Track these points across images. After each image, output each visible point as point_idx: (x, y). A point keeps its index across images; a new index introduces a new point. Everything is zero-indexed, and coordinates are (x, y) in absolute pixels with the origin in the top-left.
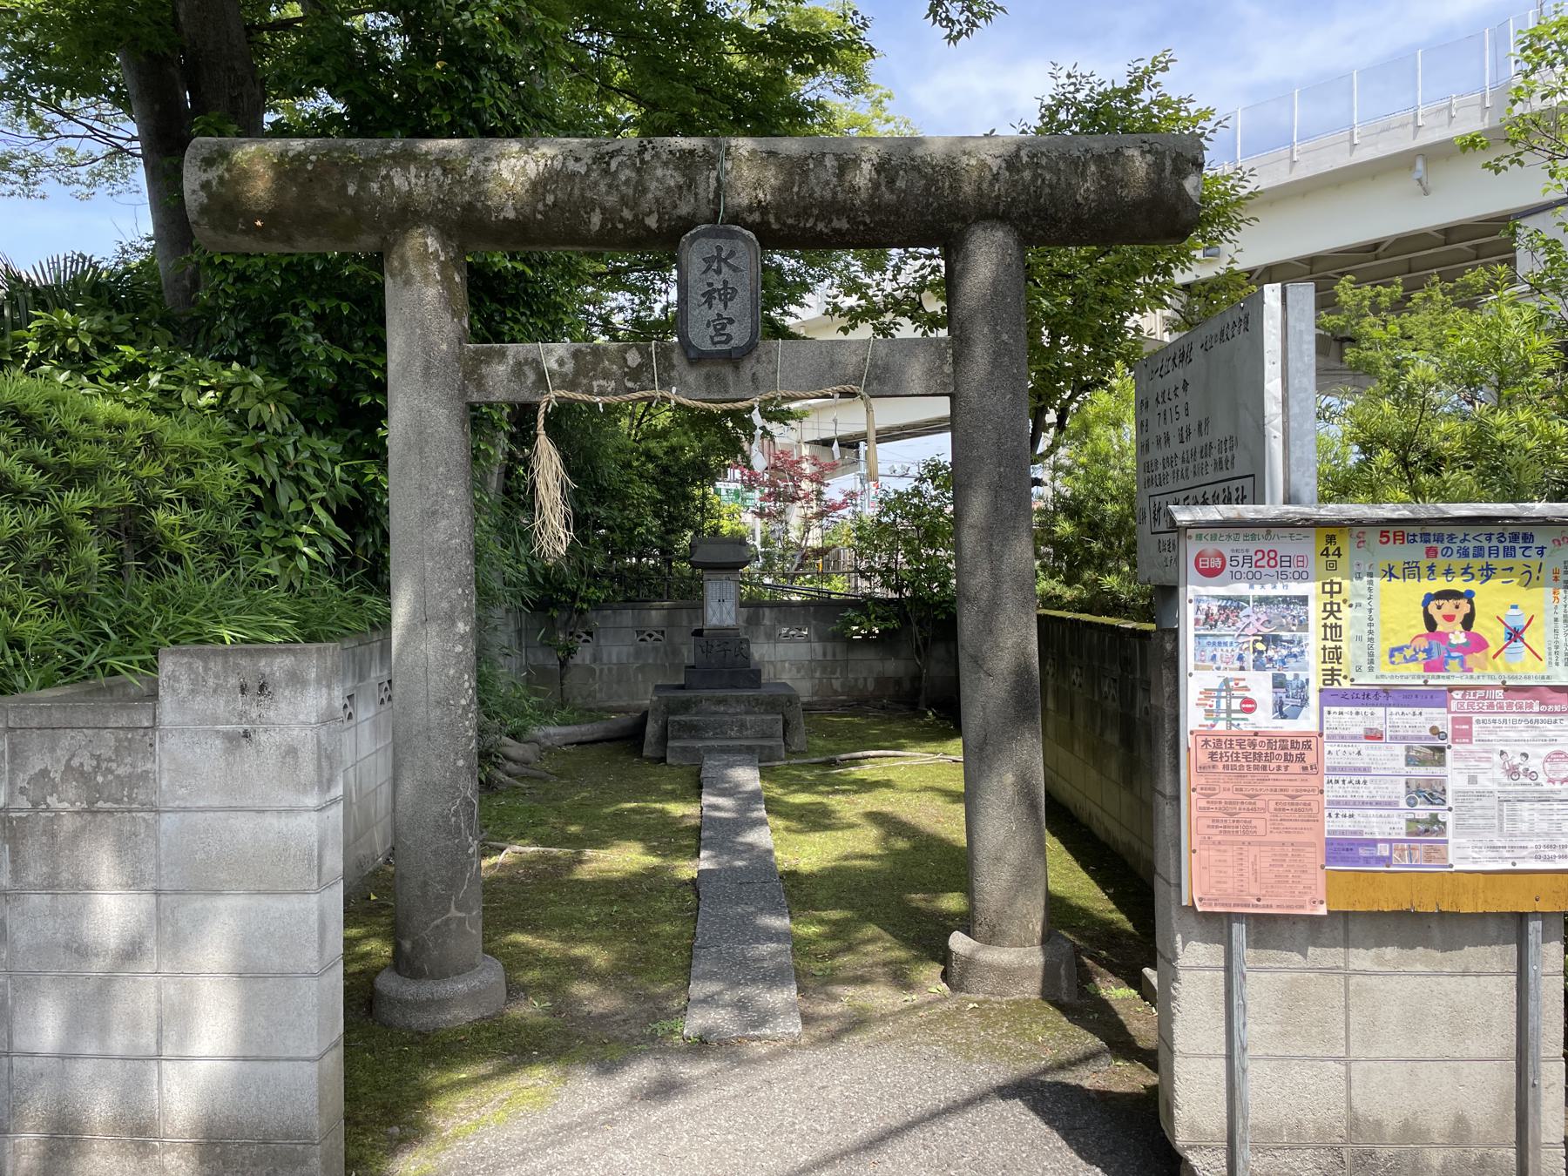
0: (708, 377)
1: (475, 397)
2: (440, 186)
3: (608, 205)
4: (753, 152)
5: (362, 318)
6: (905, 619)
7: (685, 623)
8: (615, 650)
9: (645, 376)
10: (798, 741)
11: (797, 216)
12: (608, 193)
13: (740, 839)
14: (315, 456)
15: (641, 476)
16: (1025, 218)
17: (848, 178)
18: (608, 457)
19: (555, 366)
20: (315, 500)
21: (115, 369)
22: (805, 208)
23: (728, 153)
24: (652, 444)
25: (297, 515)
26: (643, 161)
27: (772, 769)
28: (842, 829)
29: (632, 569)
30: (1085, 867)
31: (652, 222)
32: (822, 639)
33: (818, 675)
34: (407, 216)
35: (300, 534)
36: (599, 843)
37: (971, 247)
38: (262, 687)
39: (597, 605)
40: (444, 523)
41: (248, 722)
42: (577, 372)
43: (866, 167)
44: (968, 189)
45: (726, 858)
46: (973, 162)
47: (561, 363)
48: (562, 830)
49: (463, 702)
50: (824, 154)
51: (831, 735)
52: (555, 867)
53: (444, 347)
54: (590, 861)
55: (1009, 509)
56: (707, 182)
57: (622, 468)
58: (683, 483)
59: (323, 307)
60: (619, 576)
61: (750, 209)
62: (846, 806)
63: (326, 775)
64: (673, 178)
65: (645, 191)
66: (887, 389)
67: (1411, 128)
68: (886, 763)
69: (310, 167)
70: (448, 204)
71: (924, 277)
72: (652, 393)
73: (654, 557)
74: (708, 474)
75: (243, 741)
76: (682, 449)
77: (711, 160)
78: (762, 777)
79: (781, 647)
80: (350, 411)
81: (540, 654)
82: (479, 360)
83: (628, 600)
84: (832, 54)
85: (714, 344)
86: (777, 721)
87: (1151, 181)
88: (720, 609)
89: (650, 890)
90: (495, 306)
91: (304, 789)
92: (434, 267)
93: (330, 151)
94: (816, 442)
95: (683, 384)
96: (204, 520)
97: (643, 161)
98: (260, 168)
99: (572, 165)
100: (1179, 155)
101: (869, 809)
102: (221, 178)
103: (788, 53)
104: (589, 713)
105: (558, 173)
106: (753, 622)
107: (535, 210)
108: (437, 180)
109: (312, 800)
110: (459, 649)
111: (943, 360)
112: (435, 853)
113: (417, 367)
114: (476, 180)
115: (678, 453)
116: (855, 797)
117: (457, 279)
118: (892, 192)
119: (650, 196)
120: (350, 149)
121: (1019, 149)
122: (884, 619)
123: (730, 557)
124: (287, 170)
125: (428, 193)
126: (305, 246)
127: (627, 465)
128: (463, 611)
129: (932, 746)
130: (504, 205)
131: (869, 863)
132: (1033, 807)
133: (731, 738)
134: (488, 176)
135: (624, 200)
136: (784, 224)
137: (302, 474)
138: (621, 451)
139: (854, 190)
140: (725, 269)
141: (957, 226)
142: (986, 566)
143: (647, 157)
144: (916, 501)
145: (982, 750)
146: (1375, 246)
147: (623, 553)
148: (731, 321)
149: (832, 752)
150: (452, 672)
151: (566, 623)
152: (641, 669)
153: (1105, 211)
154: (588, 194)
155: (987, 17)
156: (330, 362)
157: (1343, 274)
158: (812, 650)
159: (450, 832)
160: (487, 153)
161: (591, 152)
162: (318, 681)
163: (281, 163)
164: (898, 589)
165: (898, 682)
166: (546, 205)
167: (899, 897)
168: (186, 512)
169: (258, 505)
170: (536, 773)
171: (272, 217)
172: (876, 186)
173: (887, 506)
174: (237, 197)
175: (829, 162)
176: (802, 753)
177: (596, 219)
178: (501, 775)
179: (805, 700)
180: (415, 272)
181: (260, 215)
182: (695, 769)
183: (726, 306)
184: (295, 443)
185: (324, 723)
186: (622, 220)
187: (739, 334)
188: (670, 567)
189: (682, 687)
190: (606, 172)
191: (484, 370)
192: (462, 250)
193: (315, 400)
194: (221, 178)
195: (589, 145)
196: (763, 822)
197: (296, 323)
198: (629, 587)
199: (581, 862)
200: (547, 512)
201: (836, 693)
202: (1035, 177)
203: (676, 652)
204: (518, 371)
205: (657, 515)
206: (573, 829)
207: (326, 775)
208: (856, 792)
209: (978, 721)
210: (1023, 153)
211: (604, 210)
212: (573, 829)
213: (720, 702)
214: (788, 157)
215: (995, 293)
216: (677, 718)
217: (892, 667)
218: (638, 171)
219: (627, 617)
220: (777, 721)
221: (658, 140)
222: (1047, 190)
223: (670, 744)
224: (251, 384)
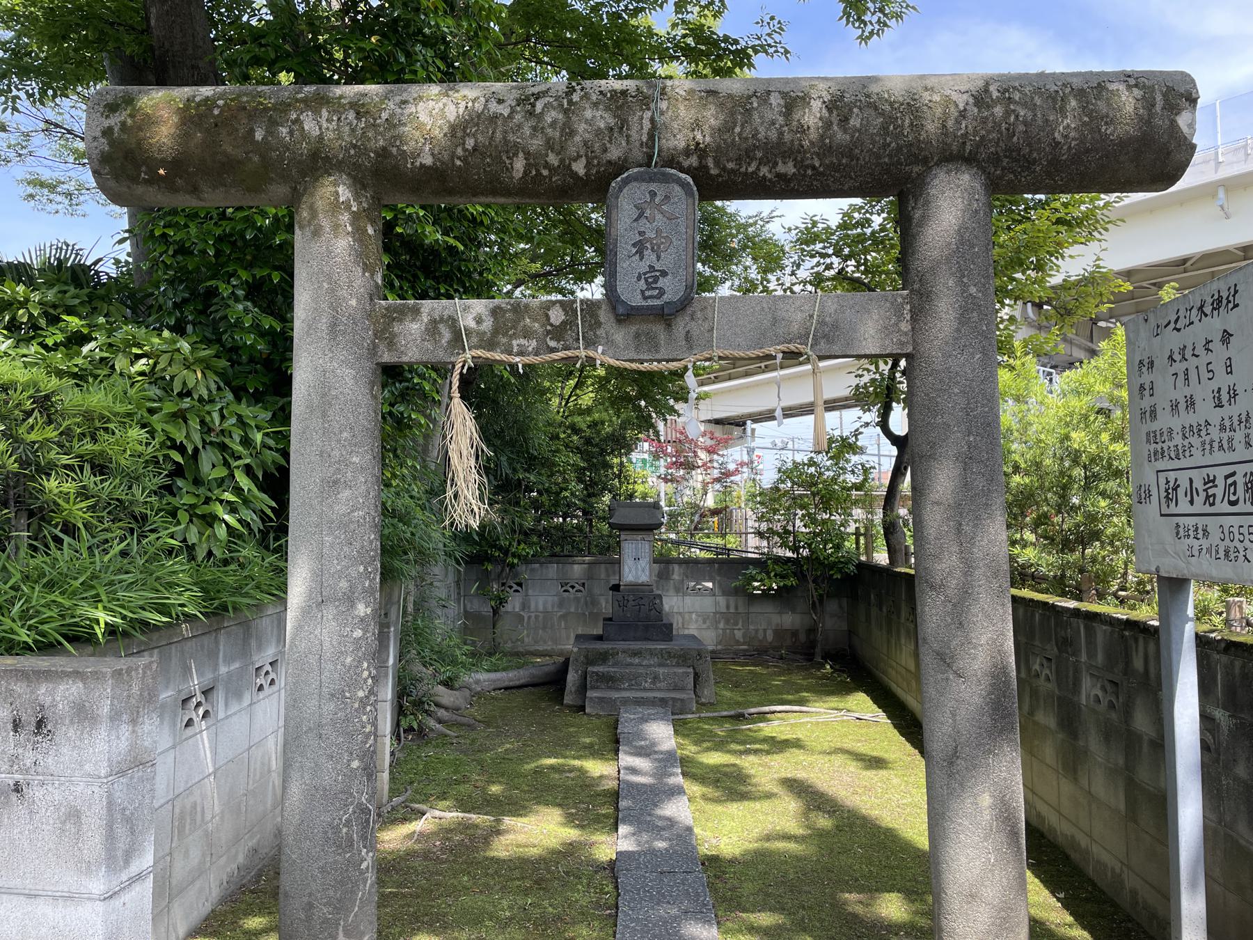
0: (637, 336)
1: (387, 358)
2: (353, 130)
3: (532, 149)
4: (691, 92)
5: (268, 272)
6: (801, 576)
7: (603, 576)
8: (541, 601)
9: (569, 335)
10: (707, 693)
11: (739, 160)
12: (532, 136)
13: (659, 812)
14: (241, 422)
15: (567, 446)
16: (995, 160)
17: (796, 116)
18: (539, 430)
19: (472, 324)
20: (238, 467)
21: (60, 338)
22: (747, 151)
23: (663, 92)
24: (577, 419)
25: (220, 482)
26: (570, 102)
27: (685, 722)
28: (760, 798)
29: (559, 528)
30: (1047, 887)
31: (579, 168)
32: (726, 593)
33: (721, 625)
34: (318, 163)
35: (221, 501)
36: (517, 808)
37: (933, 192)
38: (40, 724)
39: (525, 560)
40: (346, 493)
41: (20, 771)
42: (496, 331)
43: (816, 105)
44: (931, 127)
45: (645, 837)
46: (936, 98)
47: (479, 320)
48: (484, 789)
49: (361, 694)
50: (769, 93)
51: (737, 685)
52: (472, 838)
53: (353, 302)
54: (507, 831)
55: (980, 483)
56: (640, 125)
57: (551, 439)
58: (603, 452)
59: (254, 276)
60: (546, 533)
61: (687, 152)
62: (764, 770)
63: (121, 846)
64: (603, 119)
65: (572, 133)
66: (836, 349)
67: (1212, 163)
68: (793, 718)
69: (216, 112)
70: (361, 150)
71: (818, 273)
72: (576, 353)
73: (576, 517)
74: (623, 445)
75: (14, 797)
76: (603, 423)
77: (645, 101)
78: (676, 732)
79: (688, 600)
80: (266, 376)
81: (476, 601)
82: (395, 316)
83: (553, 555)
84: (749, 57)
85: (645, 298)
86: (687, 674)
87: (1140, 118)
88: (636, 567)
89: (567, 873)
90: (430, 282)
91: (87, 869)
92: (345, 218)
93: (239, 96)
94: (710, 421)
95: (610, 343)
96: (107, 487)
97: (570, 102)
98: (165, 114)
99: (494, 107)
100: (1170, 89)
101: (784, 775)
102: (123, 124)
103: (708, 56)
104: (519, 657)
105: (479, 116)
106: (663, 576)
107: (453, 156)
108: (350, 124)
109: (97, 885)
110: (358, 633)
111: (900, 316)
112: (323, 870)
113: (324, 322)
114: (391, 124)
115: (600, 427)
116: (766, 759)
117: (370, 231)
118: (845, 131)
119: (578, 139)
120: (259, 95)
121: (987, 84)
122: (783, 577)
123: (645, 522)
124: (192, 117)
125: (340, 138)
126: (213, 198)
127: (555, 437)
128: (365, 591)
129: (834, 701)
130: (421, 150)
131: (792, 846)
132: (1014, 834)
133: (645, 689)
134: (404, 119)
135: (549, 144)
136: (724, 169)
137: (227, 441)
138: (550, 425)
139: (803, 130)
140: (659, 216)
141: (916, 169)
142: (955, 548)
143: (575, 97)
144: (812, 470)
145: (951, 763)
146: (1184, 261)
147: (551, 514)
148: (664, 274)
149: (739, 704)
150: (349, 660)
151: (499, 575)
152: (564, 617)
153: (1087, 151)
154: (511, 137)
155: (898, 16)
156: (256, 328)
157: (1168, 282)
158: (716, 603)
159: (339, 846)
160: (405, 96)
161: (516, 94)
162: (115, 717)
163: (187, 107)
164: (795, 549)
165: (795, 634)
166: (465, 150)
167: (833, 896)
168: (89, 479)
169: (178, 471)
170: (465, 720)
171: (177, 165)
172: (828, 125)
173: (786, 473)
174: (139, 143)
175: (775, 100)
176: (710, 705)
177: (519, 165)
178: (432, 723)
179: (710, 648)
180: (326, 223)
181: (163, 163)
182: (611, 720)
183: (658, 258)
184: (222, 409)
185: (122, 773)
186: (547, 165)
187: (672, 288)
188: (591, 526)
189: (600, 638)
190: (531, 113)
191: (397, 328)
192: (378, 203)
193: (248, 368)
194: (123, 124)
195: (513, 88)
196: (679, 791)
197: (225, 290)
198: (555, 543)
199: (499, 833)
200: (460, 482)
201: (738, 643)
202: (1007, 113)
203: (594, 602)
204: (433, 329)
205: (580, 480)
206: (495, 789)
207: (121, 846)
208: (768, 753)
209: (947, 729)
210: (992, 88)
211: (528, 155)
212: (495, 789)
213: (635, 654)
214: (730, 96)
215: (962, 241)
216: (595, 669)
217: (790, 620)
218: (566, 112)
219: (552, 570)
220: (687, 674)
221: (587, 83)
222: (1021, 128)
223: (589, 694)
224: (178, 350)
